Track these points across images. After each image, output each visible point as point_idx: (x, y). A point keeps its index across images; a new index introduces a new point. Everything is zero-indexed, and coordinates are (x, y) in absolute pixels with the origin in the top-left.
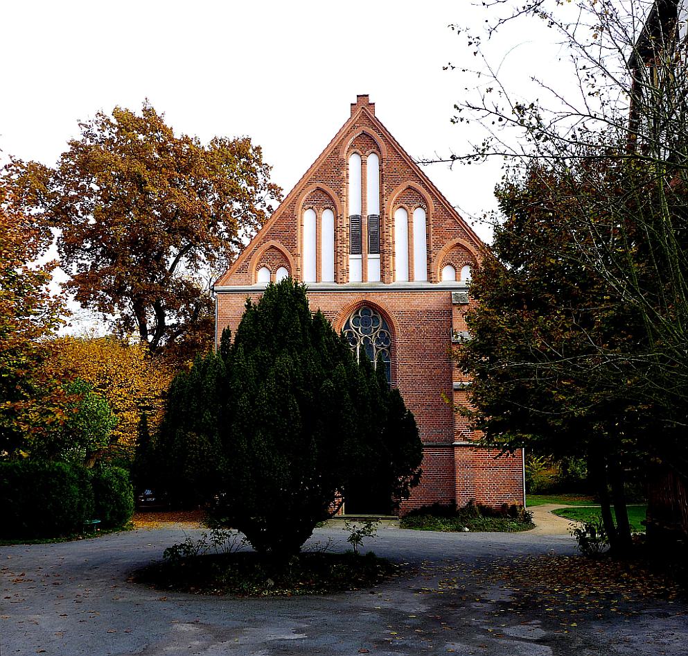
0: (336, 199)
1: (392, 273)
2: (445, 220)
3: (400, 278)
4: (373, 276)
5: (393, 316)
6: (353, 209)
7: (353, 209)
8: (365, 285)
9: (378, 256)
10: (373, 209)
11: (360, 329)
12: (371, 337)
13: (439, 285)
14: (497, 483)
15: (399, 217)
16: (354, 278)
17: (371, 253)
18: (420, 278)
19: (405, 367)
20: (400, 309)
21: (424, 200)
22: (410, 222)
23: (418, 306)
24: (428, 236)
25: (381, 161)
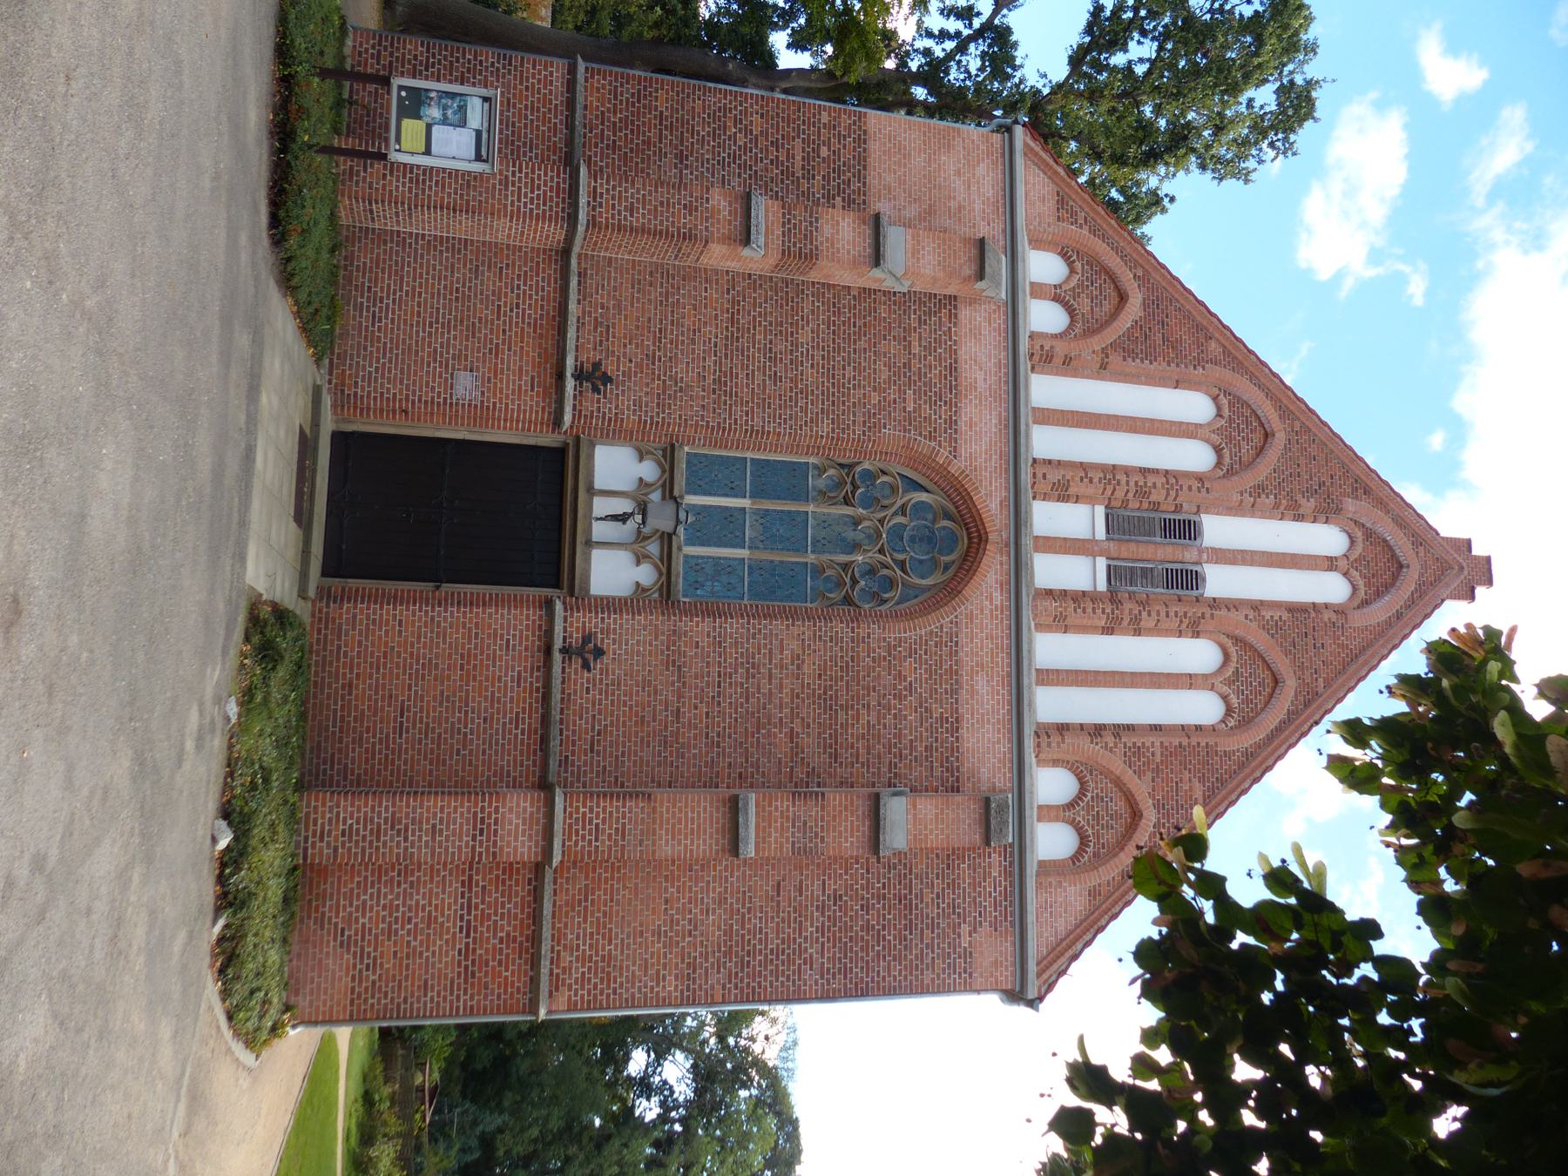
0: (1249, 479)
1: (1061, 624)
2: (1202, 780)
3: (1050, 649)
4: (1051, 571)
5: (940, 621)
6: (1218, 530)
7: (1218, 530)
8: (1029, 678)
9: (1102, 585)
10: (1220, 582)
11: (860, 491)
12: (881, 551)
13: (1027, 614)
14: (415, 932)
15: (1200, 654)
16: (1048, 517)
17: (1109, 567)
18: (1050, 705)
19: (794, 645)
20: (963, 639)
21: (1246, 723)
22: (1188, 681)
23: (973, 692)
24: (1156, 728)
25: (1339, 610)
